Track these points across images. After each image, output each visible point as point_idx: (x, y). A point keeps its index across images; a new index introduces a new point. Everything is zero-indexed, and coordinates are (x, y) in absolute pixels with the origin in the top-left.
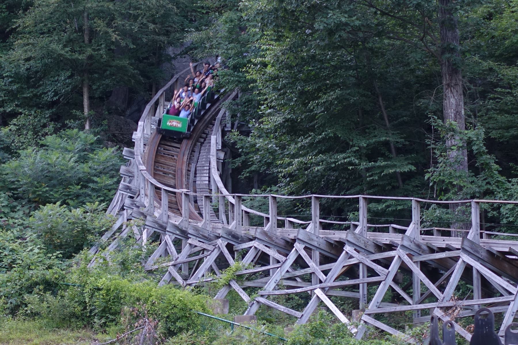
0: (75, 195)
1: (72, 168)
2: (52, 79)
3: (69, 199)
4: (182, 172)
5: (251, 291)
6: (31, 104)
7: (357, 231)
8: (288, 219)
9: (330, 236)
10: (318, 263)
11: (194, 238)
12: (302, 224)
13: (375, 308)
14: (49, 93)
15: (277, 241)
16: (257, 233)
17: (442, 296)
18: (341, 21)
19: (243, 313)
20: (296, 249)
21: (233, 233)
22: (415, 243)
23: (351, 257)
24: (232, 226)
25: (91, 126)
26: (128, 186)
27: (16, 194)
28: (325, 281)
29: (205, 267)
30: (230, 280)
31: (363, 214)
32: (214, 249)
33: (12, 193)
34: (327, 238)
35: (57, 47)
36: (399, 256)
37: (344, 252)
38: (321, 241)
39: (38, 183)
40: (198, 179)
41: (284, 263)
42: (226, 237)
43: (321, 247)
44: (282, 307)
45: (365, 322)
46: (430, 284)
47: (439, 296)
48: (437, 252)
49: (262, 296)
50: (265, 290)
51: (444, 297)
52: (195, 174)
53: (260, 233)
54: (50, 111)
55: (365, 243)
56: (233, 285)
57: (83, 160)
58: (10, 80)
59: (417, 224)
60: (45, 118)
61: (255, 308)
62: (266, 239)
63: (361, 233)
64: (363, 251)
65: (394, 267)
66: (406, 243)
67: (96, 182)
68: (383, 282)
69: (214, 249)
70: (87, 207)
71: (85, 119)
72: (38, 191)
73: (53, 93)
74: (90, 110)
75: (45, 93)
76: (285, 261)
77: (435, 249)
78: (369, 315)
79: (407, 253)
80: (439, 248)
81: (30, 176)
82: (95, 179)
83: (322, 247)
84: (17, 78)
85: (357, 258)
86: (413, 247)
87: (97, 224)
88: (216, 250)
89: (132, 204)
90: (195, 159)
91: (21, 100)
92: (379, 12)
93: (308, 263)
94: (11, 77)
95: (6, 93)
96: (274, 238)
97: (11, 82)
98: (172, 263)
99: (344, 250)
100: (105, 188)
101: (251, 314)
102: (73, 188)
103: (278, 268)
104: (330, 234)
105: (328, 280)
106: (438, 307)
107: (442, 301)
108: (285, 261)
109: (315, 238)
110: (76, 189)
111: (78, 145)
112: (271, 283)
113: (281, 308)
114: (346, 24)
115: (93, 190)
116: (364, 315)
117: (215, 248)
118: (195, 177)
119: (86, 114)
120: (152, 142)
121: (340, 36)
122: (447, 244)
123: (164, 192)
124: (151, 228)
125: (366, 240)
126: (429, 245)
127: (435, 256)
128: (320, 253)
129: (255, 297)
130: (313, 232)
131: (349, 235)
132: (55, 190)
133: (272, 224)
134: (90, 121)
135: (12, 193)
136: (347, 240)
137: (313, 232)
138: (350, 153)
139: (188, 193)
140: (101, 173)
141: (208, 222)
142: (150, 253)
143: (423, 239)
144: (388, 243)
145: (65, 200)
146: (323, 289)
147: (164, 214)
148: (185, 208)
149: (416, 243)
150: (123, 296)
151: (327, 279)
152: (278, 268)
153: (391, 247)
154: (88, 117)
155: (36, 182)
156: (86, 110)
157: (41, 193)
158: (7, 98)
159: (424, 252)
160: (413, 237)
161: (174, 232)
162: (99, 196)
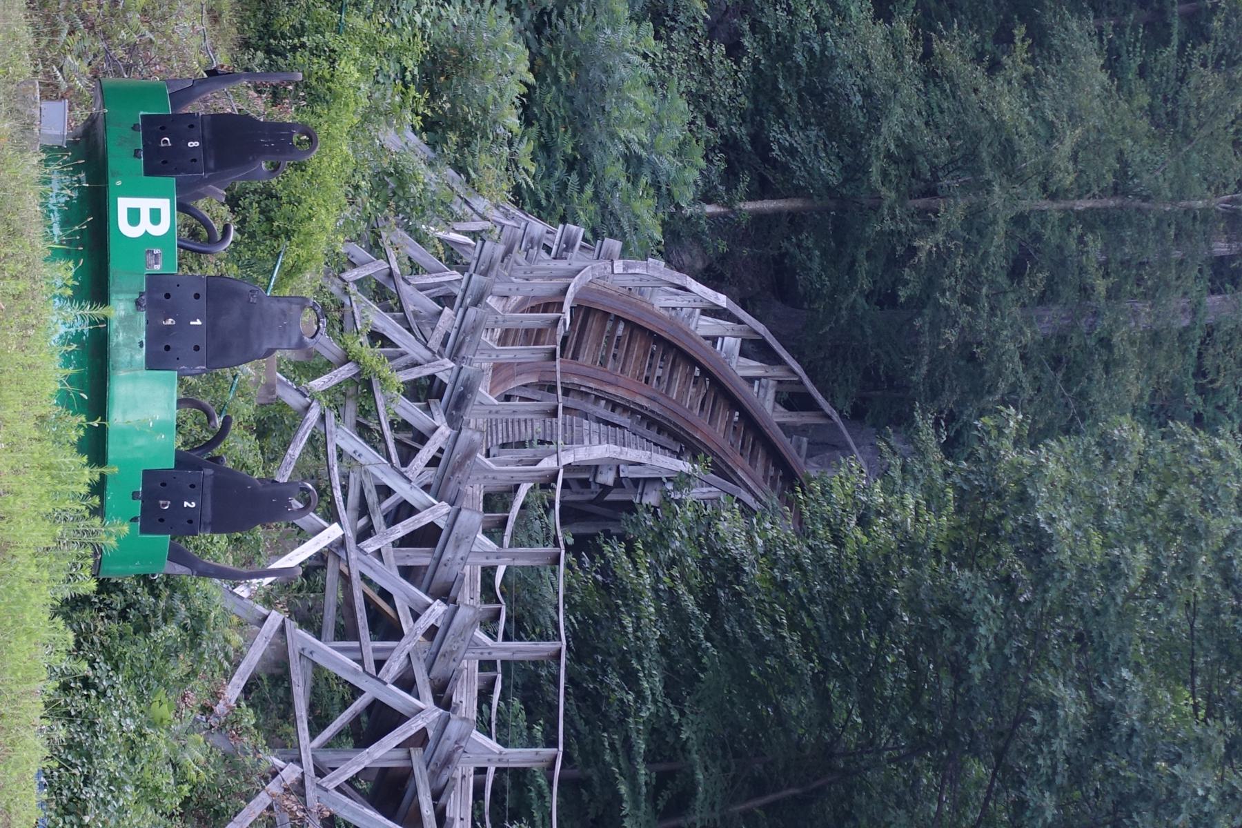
0: (550, 144)
1: (613, 136)
2: (821, 146)
3: (541, 128)
4: (610, 384)
5: (336, 398)
6: (761, 98)
7: (480, 635)
8: (500, 677)
9: (467, 590)
10: (402, 563)
11: (457, 324)
12: (492, 589)
13: (300, 646)
14: (787, 136)
15: (452, 484)
16: (470, 432)
17: (331, 786)
18: (978, 625)
19: (281, 372)
20: (434, 505)
21: (469, 396)
22: (454, 751)
23: (416, 616)
24: (485, 394)
25: (712, 217)
26: (574, 245)
27: (550, 19)
28: (361, 550)
29: (388, 326)
30: (358, 363)
31: (519, 756)
32: (430, 349)
33: (552, 10)
34: (462, 579)
35: (894, 123)
36: (423, 710)
37: (430, 601)
38: (456, 569)
39: (576, 59)
40: (595, 426)
41: (402, 474)
42: (461, 378)
43: (441, 569)
44: (298, 453)
45: (265, 618)
46: (359, 765)
47: (330, 781)
48: (435, 805)
49: (323, 418)
50: (337, 427)
51: (327, 790)
52: (607, 423)
53: (472, 441)
54: (745, 139)
55: (452, 652)
56: (346, 367)
57: (633, 163)
58: (817, 47)
59: (500, 760)
60: (729, 124)
61: (293, 399)
62: (457, 457)
63: (476, 644)
64: (434, 650)
65: (397, 698)
66: (454, 727)
67: (581, 191)
68: (360, 669)
69: (430, 349)
70: (522, 147)
71: (729, 204)
72: (558, 57)
73: (787, 144)
74: (750, 212)
75: (787, 127)
76: (406, 478)
77: (442, 801)
78: (282, 630)
79: (431, 733)
80: (444, 809)
81: (592, 41)
82: (589, 190)
83: (442, 570)
84: (822, 63)
85: (413, 631)
86: (446, 746)
87: (484, 159)
88: (428, 354)
89: (531, 241)
90: (643, 429)
91: (768, 72)
92: (1001, 743)
93: (404, 523)
94: (822, 52)
95: (785, 38)
96: (459, 475)
97: (811, 50)
98: (397, 270)
99: (435, 600)
100: (569, 212)
101: (279, 391)
102: (567, 137)
103: (389, 458)
104: (473, 590)
105: (363, 557)
106: (303, 774)
107: (318, 786)
108: (406, 478)
109: (461, 553)
110: (565, 144)
111: (667, 163)
112: (352, 442)
113: (294, 450)
114: (971, 644)
115: (564, 185)
116: (282, 617)
117: (434, 353)
118: (599, 420)
119: (742, 205)
120: (681, 329)
121: (943, 628)
122: (453, 820)
123: (562, 287)
124: (477, 255)
125: (460, 656)
126: (451, 784)
127: (425, 795)
128: (427, 567)
129: (319, 401)
130: (475, 549)
131: (471, 612)
132: (561, 100)
133: (494, 471)
134: (725, 216)
135: (552, 10)
136: (460, 510)
137: (475, 549)
138: (665, 705)
139: (561, 323)
140: (604, 207)
141: (494, 357)
142: (421, 239)
143: (463, 777)
144: (447, 815)
145: (538, 120)
146: (342, 543)
147: (512, 286)
148: (525, 318)
149: (456, 756)
150: (318, 109)
151: (365, 554)
152: (389, 458)
153: (442, 697)
154: (733, 211)
155: (578, 54)
156: (750, 206)
157: (554, 64)
158: (774, 38)
159: (434, 776)
160: (469, 747)
161: (469, 292)
162: (548, 196)
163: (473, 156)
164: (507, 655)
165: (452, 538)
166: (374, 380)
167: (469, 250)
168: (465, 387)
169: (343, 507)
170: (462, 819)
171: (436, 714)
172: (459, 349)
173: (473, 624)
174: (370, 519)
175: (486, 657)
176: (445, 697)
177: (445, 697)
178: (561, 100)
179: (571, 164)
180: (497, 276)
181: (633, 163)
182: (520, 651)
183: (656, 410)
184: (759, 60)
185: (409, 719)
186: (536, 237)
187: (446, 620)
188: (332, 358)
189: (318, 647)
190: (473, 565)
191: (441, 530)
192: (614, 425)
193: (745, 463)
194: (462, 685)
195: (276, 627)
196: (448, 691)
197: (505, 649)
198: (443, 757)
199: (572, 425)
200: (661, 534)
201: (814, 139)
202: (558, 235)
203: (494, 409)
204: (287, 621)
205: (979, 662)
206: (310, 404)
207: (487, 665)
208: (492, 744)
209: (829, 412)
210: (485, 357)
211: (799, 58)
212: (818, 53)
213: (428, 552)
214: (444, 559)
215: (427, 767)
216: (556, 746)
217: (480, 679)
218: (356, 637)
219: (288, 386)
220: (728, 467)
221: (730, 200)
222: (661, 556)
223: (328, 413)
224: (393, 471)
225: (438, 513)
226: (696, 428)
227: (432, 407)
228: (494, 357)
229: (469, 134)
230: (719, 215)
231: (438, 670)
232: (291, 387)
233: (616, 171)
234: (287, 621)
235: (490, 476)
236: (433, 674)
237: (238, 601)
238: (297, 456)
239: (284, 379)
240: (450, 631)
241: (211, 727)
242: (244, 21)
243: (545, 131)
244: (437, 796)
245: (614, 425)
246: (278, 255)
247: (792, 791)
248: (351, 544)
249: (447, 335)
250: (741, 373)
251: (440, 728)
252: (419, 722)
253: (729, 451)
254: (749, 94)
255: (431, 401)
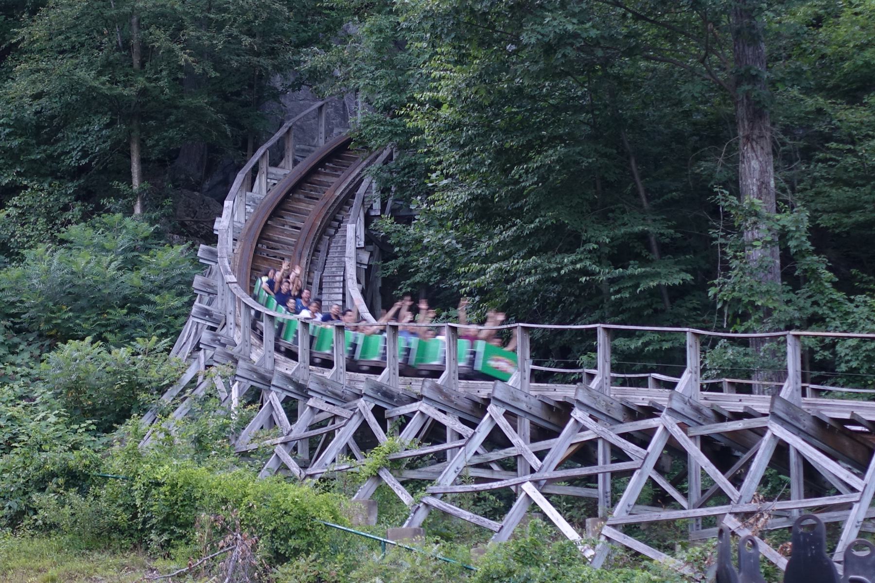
0: (118, 325)
1: (113, 279)
2: (79, 129)
3: (107, 331)
5: (415, 486)
6: (43, 171)
7: (594, 384)
9: (547, 394)
11: (319, 396)
13: (625, 514)
14: (74, 153)
15: (459, 402)
18: (565, 30)
19: (402, 523)
20: (490, 416)
21: (384, 388)
22: (691, 405)
23: (584, 429)
26: (206, 310)
27: (18, 323)
28: (540, 469)
30: (379, 469)
32: (352, 417)
33: (12, 322)
34: (543, 397)
41: (470, 439)
42: (372, 395)
45: (608, 538)
47: (733, 494)
49: (433, 495)
50: (439, 484)
51: (741, 497)
52: (321, 288)
53: (430, 388)
54: (76, 183)
55: (607, 405)
56: (384, 477)
57: (131, 265)
58: (7, 130)
59: (696, 373)
60: (66, 195)
61: (421, 515)
62: (440, 398)
63: (601, 387)
64: (604, 418)
65: (657, 444)
66: (677, 405)
67: (154, 303)
68: (638, 471)
71: (134, 196)
72: (56, 318)
76: (472, 436)
77: (726, 414)
78: (614, 526)
79: (679, 421)
80: (731, 413)
81: (41, 293)
82: (152, 297)
83: (534, 411)
85: (594, 430)
87: (153, 373)
88: (356, 418)
94: (9, 126)
96: (453, 397)
99: (571, 417)
101: (416, 525)
102: (113, 312)
104: (548, 390)
105: (545, 468)
106: (730, 513)
107: (738, 502)
108: (472, 436)
109: (523, 397)
112: (449, 474)
113: (465, 516)
114: (575, 36)
115: (148, 316)
116: (606, 527)
117: (354, 414)
119: (135, 188)
121: (564, 55)
124: (246, 381)
125: (609, 400)
126: (715, 408)
128: (531, 423)
129: (422, 497)
130: (519, 387)
131: (581, 391)
132: (83, 316)
133: (450, 373)
134: (143, 200)
135: (12, 322)
136: (577, 401)
137: (519, 387)
138: (582, 253)
141: (342, 370)
143: (706, 399)
146: (536, 483)
149: (694, 404)
150: (199, 495)
151: (542, 466)
154: (140, 194)
156: (136, 181)
157: (59, 321)
159: (707, 420)
160: (688, 394)
161: (285, 387)
162: (159, 327)
163: (150, 382)
165: (513, 403)
166: (392, 457)
168: (378, 391)
169: (499, 483)
170: (740, 400)
172: (337, 395)
174: (492, 461)
175: (608, 381)
178: (83, 316)
179: (133, 311)
180: (260, 366)
181: (131, 265)
182: (605, 356)
183: (307, 253)
186: (212, 337)
187: (501, 404)
188: (374, 487)
189: (625, 501)
190: (530, 388)
191: (376, 405)
192: (321, 283)
193: (329, 191)
196: (552, 404)
201: (74, 135)
202: (199, 321)
203: (392, 371)
204: (608, 522)
205: (586, 30)
208: (686, 375)
211: (15, 143)
212: (11, 130)
213: (521, 422)
214: (526, 409)
215: (701, 425)
217: (729, 392)
218: (596, 475)
219: (413, 518)
220: (335, 201)
221: (131, 196)
222: (463, 253)
224: (468, 446)
225: (365, 406)
226: (313, 224)
228: (342, 370)
229: (135, 386)
232: (413, 518)
233: (133, 278)
234: (608, 522)
235: (453, 375)
236: (622, 420)
239: (407, 522)
240: (593, 406)
241: (703, 578)
243: (109, 329)
244: (721, 418)
245: (321, 283)
248: (536, 476)
249: (591, 416)
250: (264, 192)
251: (675, 415)
252: (675, 429)
253: (325, 201)
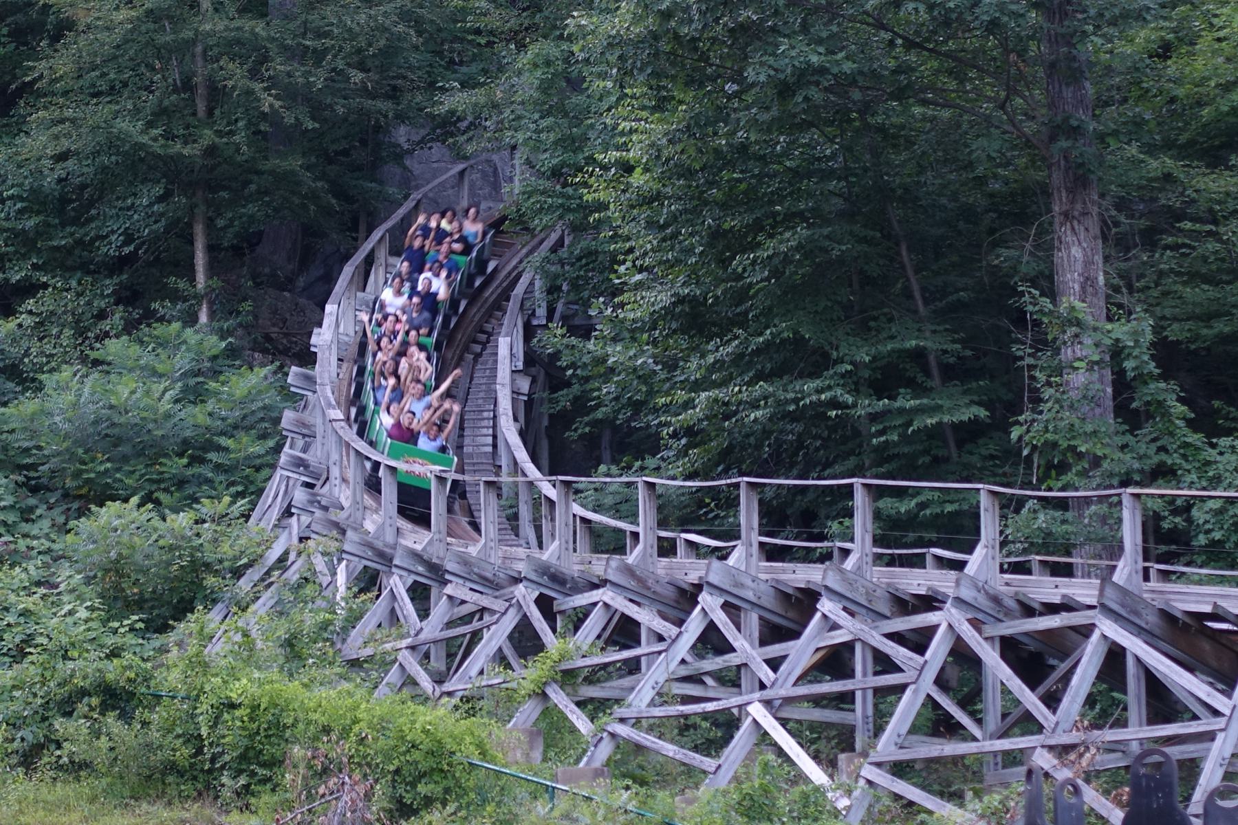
2: (119, 204)
3: (159, 489)
6: (69, 263)
9: (783, 577)
11: (461, 581)
13: (893, 748)
14: (114, 238)
15: (658, 589)
20: (703, 609)
21: (552, 570)
22: (987, 593)
23: (835, 627)
25: (212, 315)
26: (301, 459)
27: (34, 478)
28: (773, 684)
30: (545, 684)
32: (507, 610)
33: (25, 476)
34: (777, 581)
36: (950, 626)
38: (763, 587)
41: (674, 641)
45: (869, 782)
46: (1023, 691)
47: (1046, 719)
49: (622, 720)
51: (1057, 723)
53: (618, 569)
54: (116, 280)
55: (867, 593)
57: (194, 395)
60: (102, 296)
61: (605, 750)
62: (631, 584)
64: (864, 611)
65: (938, 649)
66: (967, 593)
67: (226, 449)
69: (507, 610)
70: (204, 510)
71: (199, 298)
73: (121, 238)
76: (678, 636)
77: (1036, 606)
78: (879, 765)
79: (969, 616)
81: (67, 436)
82: (224, 441)
84: (35, 201)
85: (849, 628)
86: (983, 602)
87: (226, 549)
88: (512, 612)
93: (731, 640)
94: (21, 199)
96: (650, 582)
101: (597, 764)
102: (169, 463)
104: (784, 571)
105: (780, 682)
106: (1043, 746)
107: (1054, 730)
109: (749, 582)
110: (176, 465)
113: (668, 750)
115: (218, 467)
116: (866, 766)
119: (200, 286)
121: (806, 99)
122: (1064, 596)
123: (388, 473)
124: (357, 559)
126: (1021, 598)
128: (761, 618)
129: (606, 724)
130: (743, 568)
131: (830, 573)
132: (127, 468)
133: (645, 548)
134: (211, 304)
135: (25, 476)
136: (826, 587)
137: (743, 568)
141: (492, 544)
143: (1007, 584)
146: (768, 703)
149: (991, 592)
150: (290, 721)
151: (776, 680)
152: (660, 653)
154: (206, 294)
155: (80, 451)
156: (201, 277)
157: (92, 475)
159: (1009, 613)
160: (982, 578)
161: (412, 568)
164: (869, 539)
165: (735, 591)
167: (351, 566)
168: (544, 574)
171: (953, 611)
173: (842, 571)
175: (870, 559)
176: (913, 600)
177: (913, 600)
179: (196, 460)
182: (864, 524)
184: (33, 265)
185: (525, 615)
191: (415, 582)
194: (1039, 593)
195: (878, 771)
197: (863, 540)
198: (992, 605)
199: (474, 464)
200: (639, 377)
202: (290, 474)
205: (837, 63)
206: (610, 733)
207: (666, 549)
209: (414, 203)
210: (493, 552)
211: (30, 223)
212: (24, 205)
213: (746, 616)
216: (851, 485)
217: (1041, 575)
219: (592, 755)
221: (195, 297)
223: (618, 716)
227: (563, 608)
230: (210, 308)
231: (884, 608)
234: (870, 760)
235: (649, 550)
236: (889, 614)
237: (853, 809)
238: (675, 748)
240: (848, 595)
242: (183, 798)
243: (162, 486)
244: (1028, 611)
246: (471, 764)
247: (904, 253)
254: (67, 275)
255: (555, 609)
